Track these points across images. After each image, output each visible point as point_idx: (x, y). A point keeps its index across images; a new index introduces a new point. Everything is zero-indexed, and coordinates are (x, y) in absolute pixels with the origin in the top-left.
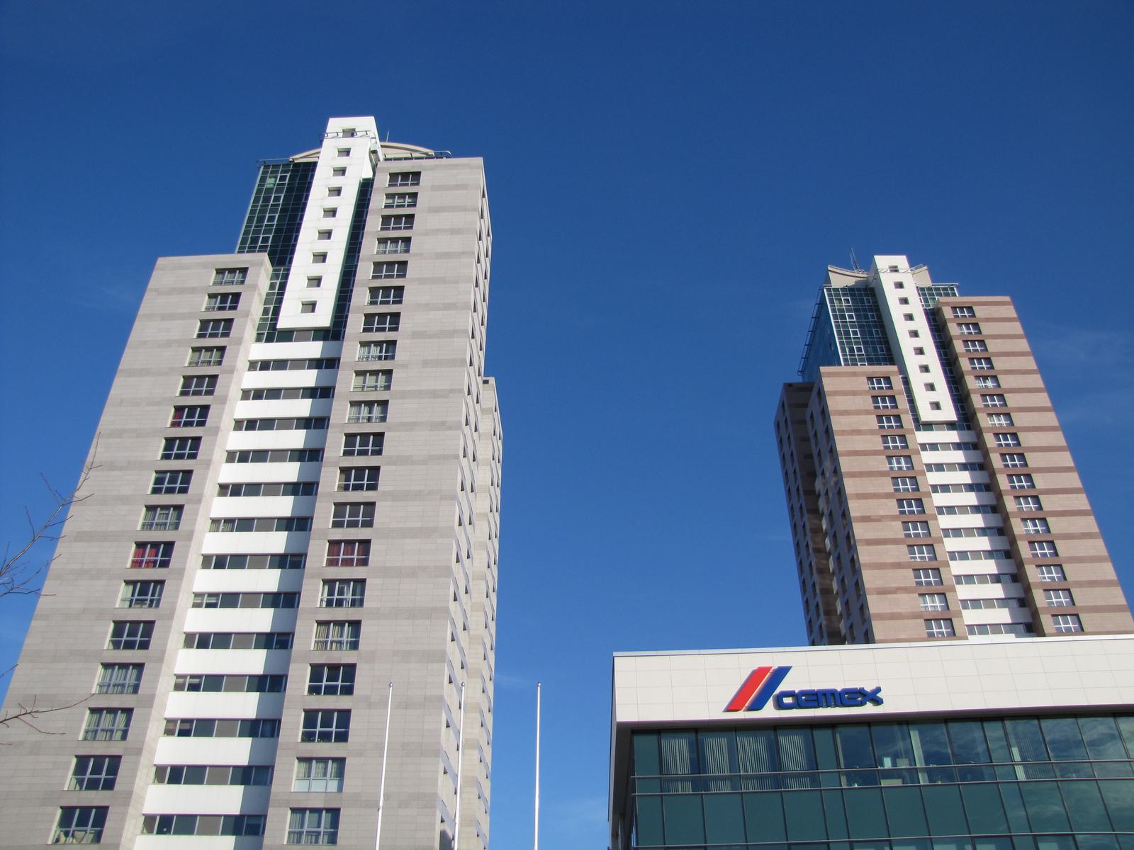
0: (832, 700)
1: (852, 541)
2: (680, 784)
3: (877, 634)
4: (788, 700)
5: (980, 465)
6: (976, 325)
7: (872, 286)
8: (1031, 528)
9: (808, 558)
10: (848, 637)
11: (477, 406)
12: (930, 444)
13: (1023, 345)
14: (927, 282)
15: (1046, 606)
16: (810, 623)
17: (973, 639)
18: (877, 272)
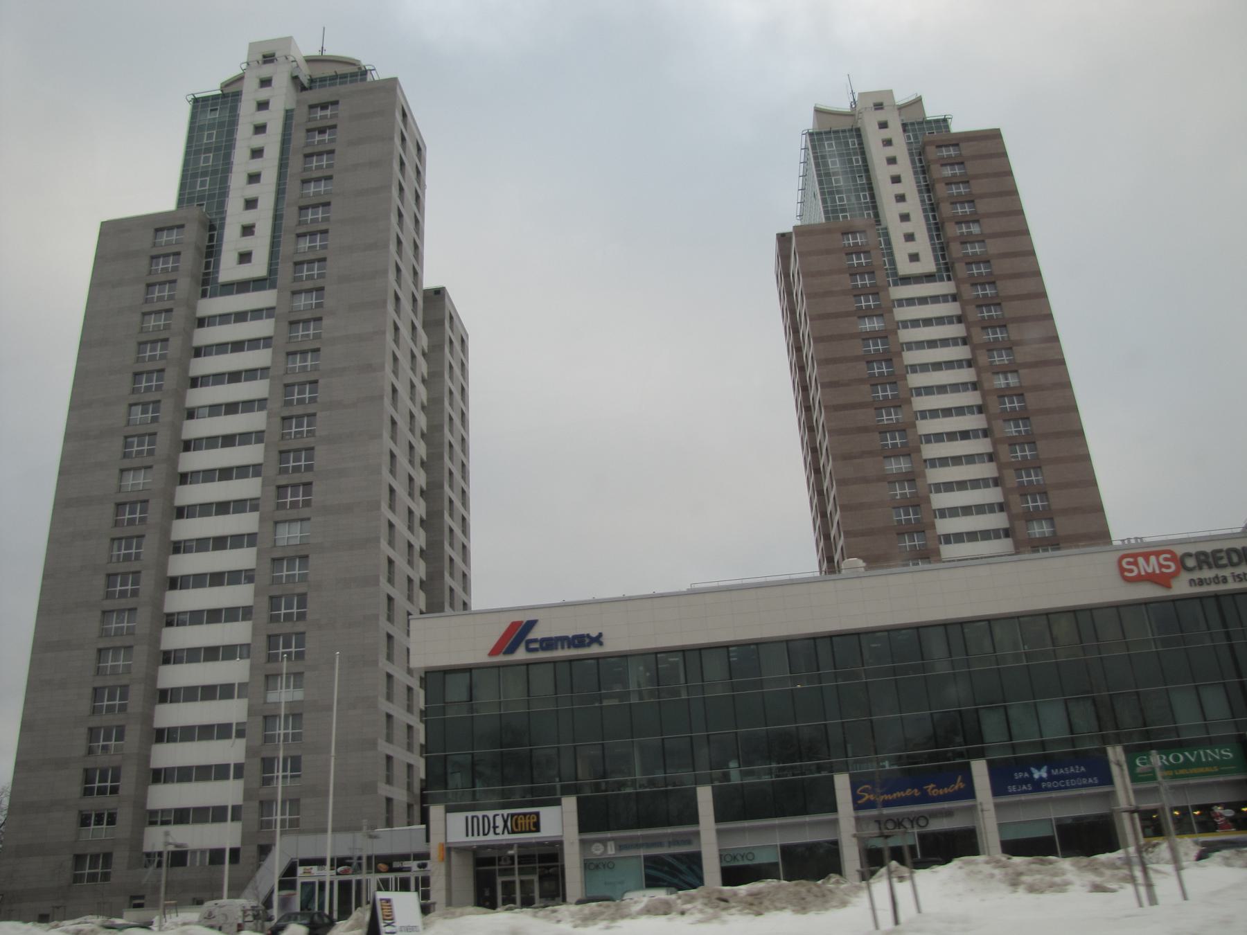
4: (536, 645)
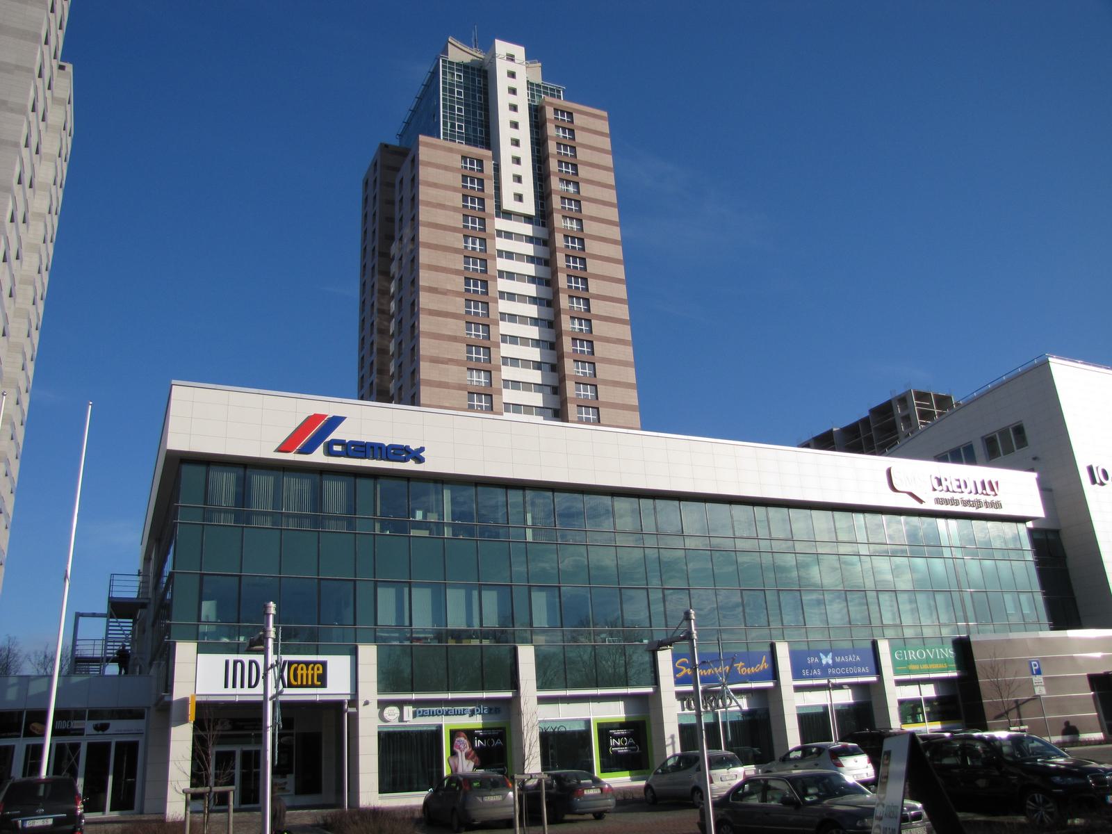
0: (379, 454)
1: (416, 309)
2: (222, 515)
3: (423, 400)
4: (337, 448)
5: (545, 261)
6: (572, 132)
7: (486, 68)
8: (577, 326)
9: (371, 318)
10: (396, 397)
11: (48, 93)
12: (505, 232)
13: (608, 160)
14: (538, 79)
15: (575, 396)
16: (362, 379)
17: (507, 416)
18: (494, 56)
